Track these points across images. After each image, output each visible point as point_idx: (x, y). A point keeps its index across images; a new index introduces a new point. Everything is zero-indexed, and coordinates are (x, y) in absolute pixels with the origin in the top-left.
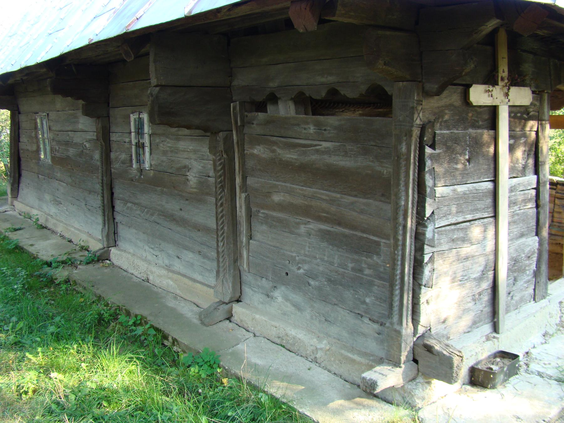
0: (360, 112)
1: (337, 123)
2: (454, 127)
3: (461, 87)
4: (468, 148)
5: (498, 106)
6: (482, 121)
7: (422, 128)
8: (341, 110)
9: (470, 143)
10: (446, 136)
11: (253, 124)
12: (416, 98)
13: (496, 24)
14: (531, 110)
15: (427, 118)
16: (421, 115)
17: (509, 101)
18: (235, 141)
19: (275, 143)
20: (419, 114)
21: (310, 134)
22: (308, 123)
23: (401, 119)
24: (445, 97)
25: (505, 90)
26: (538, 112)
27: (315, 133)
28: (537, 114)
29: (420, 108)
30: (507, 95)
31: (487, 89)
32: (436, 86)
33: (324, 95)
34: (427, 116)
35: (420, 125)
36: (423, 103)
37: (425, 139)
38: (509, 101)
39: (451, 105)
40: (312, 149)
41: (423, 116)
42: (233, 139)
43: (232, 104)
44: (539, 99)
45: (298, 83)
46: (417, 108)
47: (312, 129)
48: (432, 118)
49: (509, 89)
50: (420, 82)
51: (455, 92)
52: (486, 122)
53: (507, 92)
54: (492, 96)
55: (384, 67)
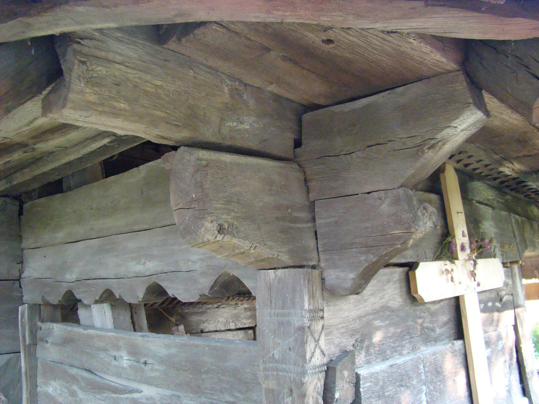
0: (246, 306)
1: (163, 352)
2: (397, 350)
3: (400, 270)
4: (424, 387)
5: (463, 296)
6: (441, 327)
7: (326, 372)
8: (216, 306)
9: (426, 377)
10: (380, 377)
11: (47, 342)
12: (306, 306)
13: (473, 124)
14: (504, 293)
15: (337, 346)
16: (322, 342)
17: (478, 285)
18: (23, 370)
19: (74, 379)
20: (317, 341)
21: (122, 368)
22: (118, 349)
23: (277, 357)
24: (372, 294)
25: (470, 266)
26: (512, 295)
27: (130, 367)
28: (511, 298)
29: (318, 326)
30: (473, 274)
31: (444, 269)
32: (352, 276)
33: (142, 297)
34: (336, 341)
35: (321, 366)
36: (326, 315)
37: (337, 395)
38: (478, 285)
39: (385, 308)
40: (127, 398)
41: (329, 342)
42: (20, 367)
43: (20, 307)
44: (510, 274)
45: (102, 273)
46: (312, 328)
47: (126, 361)
48: (348, 343)
49: (475, 264)
50: (314, 267)
51: (389, 281)
52: (446, 327)
53: (472, 269)
54: (452, 280)
55: (220, 237)
